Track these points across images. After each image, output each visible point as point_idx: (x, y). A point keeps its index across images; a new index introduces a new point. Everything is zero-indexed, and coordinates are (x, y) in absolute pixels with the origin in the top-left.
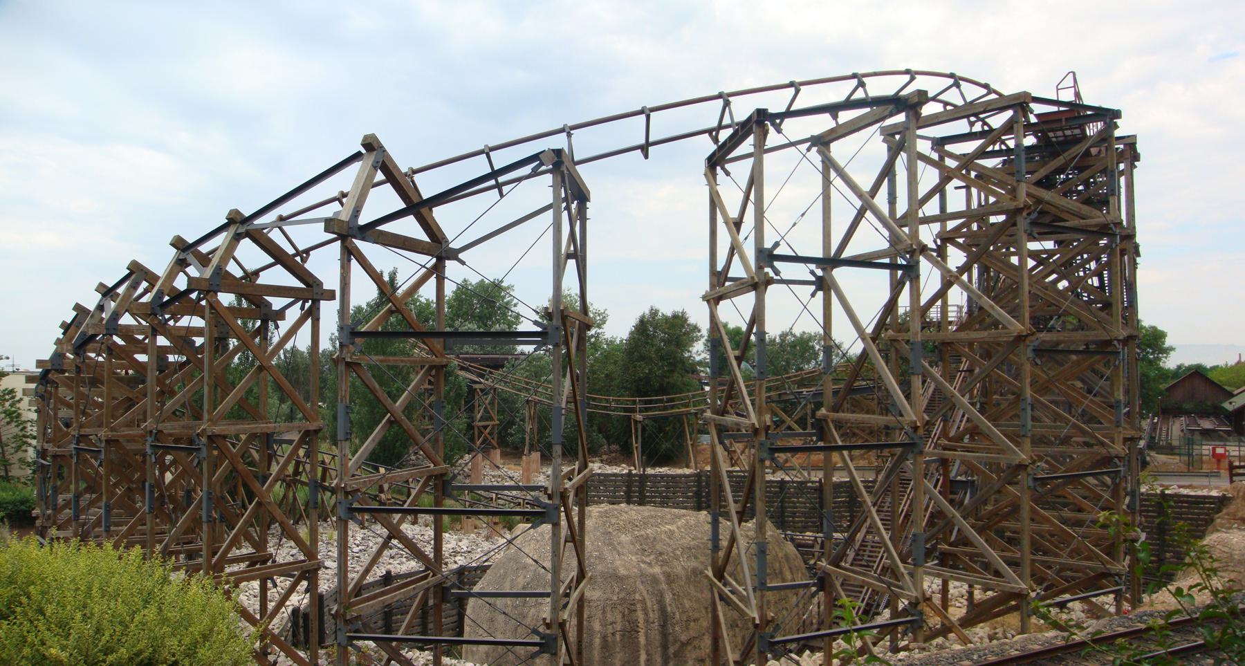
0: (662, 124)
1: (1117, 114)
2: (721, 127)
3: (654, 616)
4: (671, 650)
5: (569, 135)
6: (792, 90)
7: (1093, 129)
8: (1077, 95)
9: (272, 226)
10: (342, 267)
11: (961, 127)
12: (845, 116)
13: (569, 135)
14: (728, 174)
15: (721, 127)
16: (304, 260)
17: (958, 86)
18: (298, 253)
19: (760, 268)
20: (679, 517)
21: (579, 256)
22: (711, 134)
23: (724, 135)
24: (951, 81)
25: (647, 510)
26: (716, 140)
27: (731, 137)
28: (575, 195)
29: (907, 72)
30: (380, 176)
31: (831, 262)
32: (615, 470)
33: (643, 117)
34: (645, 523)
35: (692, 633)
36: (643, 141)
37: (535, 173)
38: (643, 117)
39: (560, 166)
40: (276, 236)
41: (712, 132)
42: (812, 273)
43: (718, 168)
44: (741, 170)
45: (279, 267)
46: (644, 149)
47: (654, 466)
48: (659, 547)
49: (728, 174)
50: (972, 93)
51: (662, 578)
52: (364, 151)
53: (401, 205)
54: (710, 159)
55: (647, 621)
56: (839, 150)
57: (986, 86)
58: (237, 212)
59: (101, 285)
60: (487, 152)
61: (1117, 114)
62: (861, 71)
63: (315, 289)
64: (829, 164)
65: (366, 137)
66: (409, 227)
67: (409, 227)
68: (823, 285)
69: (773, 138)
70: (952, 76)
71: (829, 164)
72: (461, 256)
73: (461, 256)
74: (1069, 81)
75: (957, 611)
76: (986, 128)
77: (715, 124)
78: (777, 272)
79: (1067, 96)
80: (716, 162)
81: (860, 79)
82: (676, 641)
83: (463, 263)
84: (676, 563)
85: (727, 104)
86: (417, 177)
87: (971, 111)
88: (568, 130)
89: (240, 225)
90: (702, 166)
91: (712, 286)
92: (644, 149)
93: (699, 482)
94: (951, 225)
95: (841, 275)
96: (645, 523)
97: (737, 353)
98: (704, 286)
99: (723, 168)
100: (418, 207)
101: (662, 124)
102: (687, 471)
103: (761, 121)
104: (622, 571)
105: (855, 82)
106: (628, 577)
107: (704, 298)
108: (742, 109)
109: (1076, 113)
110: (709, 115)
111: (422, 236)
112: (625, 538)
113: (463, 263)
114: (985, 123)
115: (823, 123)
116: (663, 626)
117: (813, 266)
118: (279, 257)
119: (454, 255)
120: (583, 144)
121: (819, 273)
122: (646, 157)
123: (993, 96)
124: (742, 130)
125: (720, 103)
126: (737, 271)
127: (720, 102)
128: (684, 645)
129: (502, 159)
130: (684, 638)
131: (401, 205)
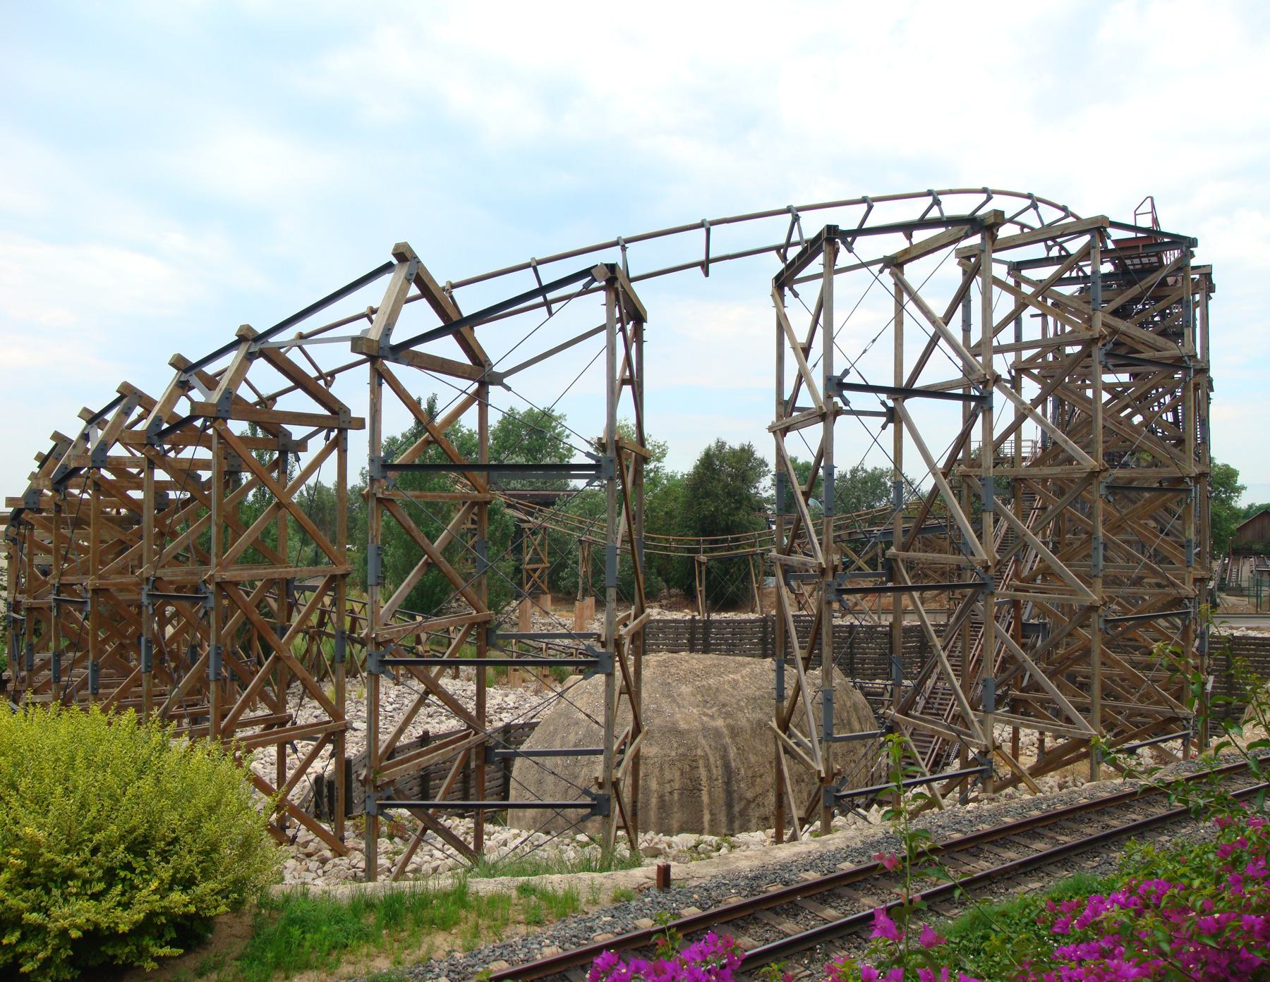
0: (724, 240)
1: (1193, 242)
2: (789, 244)
3: (717, 772)
4: (737, 809)
5: (624, 249)
6: (864, 207)
7: (1170, 257)
8: (1155, 221)
9: (290, 345)
10: (372, 392)
11: (1038, 251)
12: (920, 236)
13: (624, 249)
14: (796, 295)
15: (789, 244)
16: (328, 384)
17: (1036, 208)
18: (321, 376)
19: (828, 397)
20: (744, 665)
21: (635, 381)
22: (778, 252)
23: (793, 253)
24: (1028, 202)
25: (710, 659)
26: (784, 258)
27: (800, 255)
28: (632, 315)
29: (984, 190)
30: (414, 290)
31: (902, 392)
32: (677, 615)
33: (703, 230)
34: (707, 673)
35: (758, 790)
36: (703, 258)
37: (586, 291)
38: (703, 230)
39: (614, 282)
40: (295, 356)
41: (781, 250)
42: (883, 403)
43: (786, 289)
44: (810, 292)
45: (299, 392)
46: (705, 265)
47: (719, 611)
48: (722, 698)
49: (796, 295)
50: (1050, 215)
51: (725, 731)
52: (395, 261)
53: (439, 323)
54: (777, 278)
55: (710, 778)
56: (913, 272)
57: (1064, 209)
58: (249, 328)
59: (86, 410)
60: (534, 265)
61: (1193, 242)
62: (936, 188)
63: (342, 417)
64: (902, 287)
65: (397, 246)
66: (448, 348)
67: (448, 348)
68: (894, 416)
69: (844, 258)
70: (1029, 196)
71: (902, 287)
72: (506, 381)
73: (506, 381)
74: (1147, 207)
75: (1028, 760)
76: (1063, 253)
77: (783, 241)
78: (846, 403)
79: (1145, 222)
80: (783, 282)
81: (935, 197)
82: (741, 799)
83: (509, 389)
84: (740, 715)
85: (796, 219)
86: (455, 292)
87: (1049, 234)
88: (622, 244)
89: (252, 343)
90: (769, 286)
91: (779, 416)
92: (705, 265)
93: (765, 627)
94: (1026, 354)
95: (913, 406)
96: (707, 673)
97: (804, 488)
98: (771, 416)
99: (791, 289)
100: (457, 325)
101: (724, 240)
102: (752, 616)
103: (832, 238)
104: (683, 725)
105: (929, 200)
106: (689, 731)
107: (770, 429)
108: (812, 226)
109: (1154, 240)
110: (776, 230)
111: (463, 358)
112: (686, 689)
113: (509, 389)
114: (1062, 248)
115: (895, 243)
116: (728, 783)
117: (883, 397)
118: (299, 380)
119: (498, 379)
120: (639, 259)
121: (891, 403)
122: (707, 274)
123: (1071, 219)
124: (811, 249)
125: (788, 218)
126: (805, 400)
127: (789, 217)
128: (749, 802)
129: (550, 274)
130: (749, 795)
131: (439, 323)
